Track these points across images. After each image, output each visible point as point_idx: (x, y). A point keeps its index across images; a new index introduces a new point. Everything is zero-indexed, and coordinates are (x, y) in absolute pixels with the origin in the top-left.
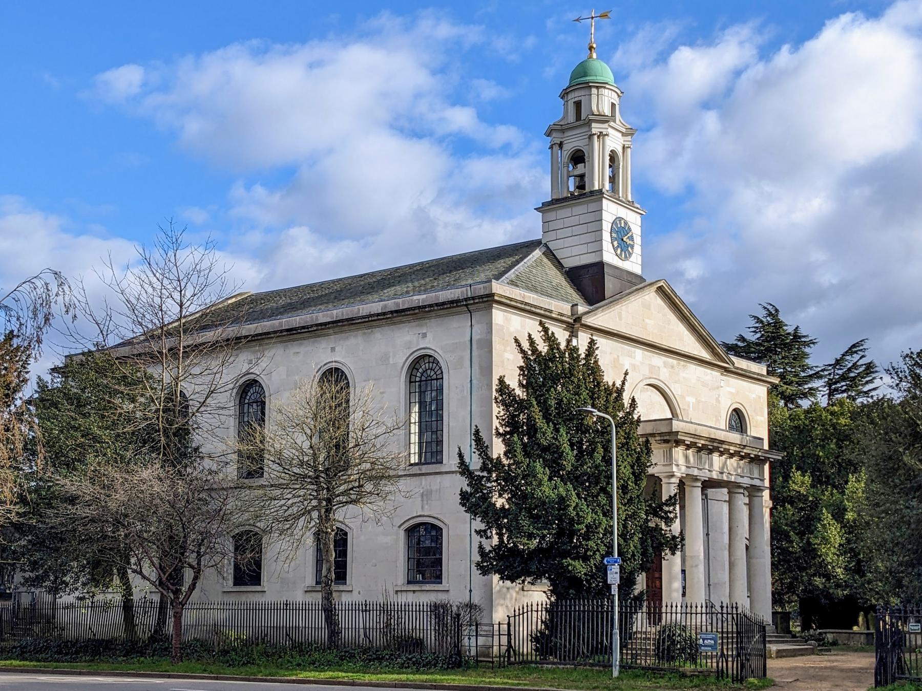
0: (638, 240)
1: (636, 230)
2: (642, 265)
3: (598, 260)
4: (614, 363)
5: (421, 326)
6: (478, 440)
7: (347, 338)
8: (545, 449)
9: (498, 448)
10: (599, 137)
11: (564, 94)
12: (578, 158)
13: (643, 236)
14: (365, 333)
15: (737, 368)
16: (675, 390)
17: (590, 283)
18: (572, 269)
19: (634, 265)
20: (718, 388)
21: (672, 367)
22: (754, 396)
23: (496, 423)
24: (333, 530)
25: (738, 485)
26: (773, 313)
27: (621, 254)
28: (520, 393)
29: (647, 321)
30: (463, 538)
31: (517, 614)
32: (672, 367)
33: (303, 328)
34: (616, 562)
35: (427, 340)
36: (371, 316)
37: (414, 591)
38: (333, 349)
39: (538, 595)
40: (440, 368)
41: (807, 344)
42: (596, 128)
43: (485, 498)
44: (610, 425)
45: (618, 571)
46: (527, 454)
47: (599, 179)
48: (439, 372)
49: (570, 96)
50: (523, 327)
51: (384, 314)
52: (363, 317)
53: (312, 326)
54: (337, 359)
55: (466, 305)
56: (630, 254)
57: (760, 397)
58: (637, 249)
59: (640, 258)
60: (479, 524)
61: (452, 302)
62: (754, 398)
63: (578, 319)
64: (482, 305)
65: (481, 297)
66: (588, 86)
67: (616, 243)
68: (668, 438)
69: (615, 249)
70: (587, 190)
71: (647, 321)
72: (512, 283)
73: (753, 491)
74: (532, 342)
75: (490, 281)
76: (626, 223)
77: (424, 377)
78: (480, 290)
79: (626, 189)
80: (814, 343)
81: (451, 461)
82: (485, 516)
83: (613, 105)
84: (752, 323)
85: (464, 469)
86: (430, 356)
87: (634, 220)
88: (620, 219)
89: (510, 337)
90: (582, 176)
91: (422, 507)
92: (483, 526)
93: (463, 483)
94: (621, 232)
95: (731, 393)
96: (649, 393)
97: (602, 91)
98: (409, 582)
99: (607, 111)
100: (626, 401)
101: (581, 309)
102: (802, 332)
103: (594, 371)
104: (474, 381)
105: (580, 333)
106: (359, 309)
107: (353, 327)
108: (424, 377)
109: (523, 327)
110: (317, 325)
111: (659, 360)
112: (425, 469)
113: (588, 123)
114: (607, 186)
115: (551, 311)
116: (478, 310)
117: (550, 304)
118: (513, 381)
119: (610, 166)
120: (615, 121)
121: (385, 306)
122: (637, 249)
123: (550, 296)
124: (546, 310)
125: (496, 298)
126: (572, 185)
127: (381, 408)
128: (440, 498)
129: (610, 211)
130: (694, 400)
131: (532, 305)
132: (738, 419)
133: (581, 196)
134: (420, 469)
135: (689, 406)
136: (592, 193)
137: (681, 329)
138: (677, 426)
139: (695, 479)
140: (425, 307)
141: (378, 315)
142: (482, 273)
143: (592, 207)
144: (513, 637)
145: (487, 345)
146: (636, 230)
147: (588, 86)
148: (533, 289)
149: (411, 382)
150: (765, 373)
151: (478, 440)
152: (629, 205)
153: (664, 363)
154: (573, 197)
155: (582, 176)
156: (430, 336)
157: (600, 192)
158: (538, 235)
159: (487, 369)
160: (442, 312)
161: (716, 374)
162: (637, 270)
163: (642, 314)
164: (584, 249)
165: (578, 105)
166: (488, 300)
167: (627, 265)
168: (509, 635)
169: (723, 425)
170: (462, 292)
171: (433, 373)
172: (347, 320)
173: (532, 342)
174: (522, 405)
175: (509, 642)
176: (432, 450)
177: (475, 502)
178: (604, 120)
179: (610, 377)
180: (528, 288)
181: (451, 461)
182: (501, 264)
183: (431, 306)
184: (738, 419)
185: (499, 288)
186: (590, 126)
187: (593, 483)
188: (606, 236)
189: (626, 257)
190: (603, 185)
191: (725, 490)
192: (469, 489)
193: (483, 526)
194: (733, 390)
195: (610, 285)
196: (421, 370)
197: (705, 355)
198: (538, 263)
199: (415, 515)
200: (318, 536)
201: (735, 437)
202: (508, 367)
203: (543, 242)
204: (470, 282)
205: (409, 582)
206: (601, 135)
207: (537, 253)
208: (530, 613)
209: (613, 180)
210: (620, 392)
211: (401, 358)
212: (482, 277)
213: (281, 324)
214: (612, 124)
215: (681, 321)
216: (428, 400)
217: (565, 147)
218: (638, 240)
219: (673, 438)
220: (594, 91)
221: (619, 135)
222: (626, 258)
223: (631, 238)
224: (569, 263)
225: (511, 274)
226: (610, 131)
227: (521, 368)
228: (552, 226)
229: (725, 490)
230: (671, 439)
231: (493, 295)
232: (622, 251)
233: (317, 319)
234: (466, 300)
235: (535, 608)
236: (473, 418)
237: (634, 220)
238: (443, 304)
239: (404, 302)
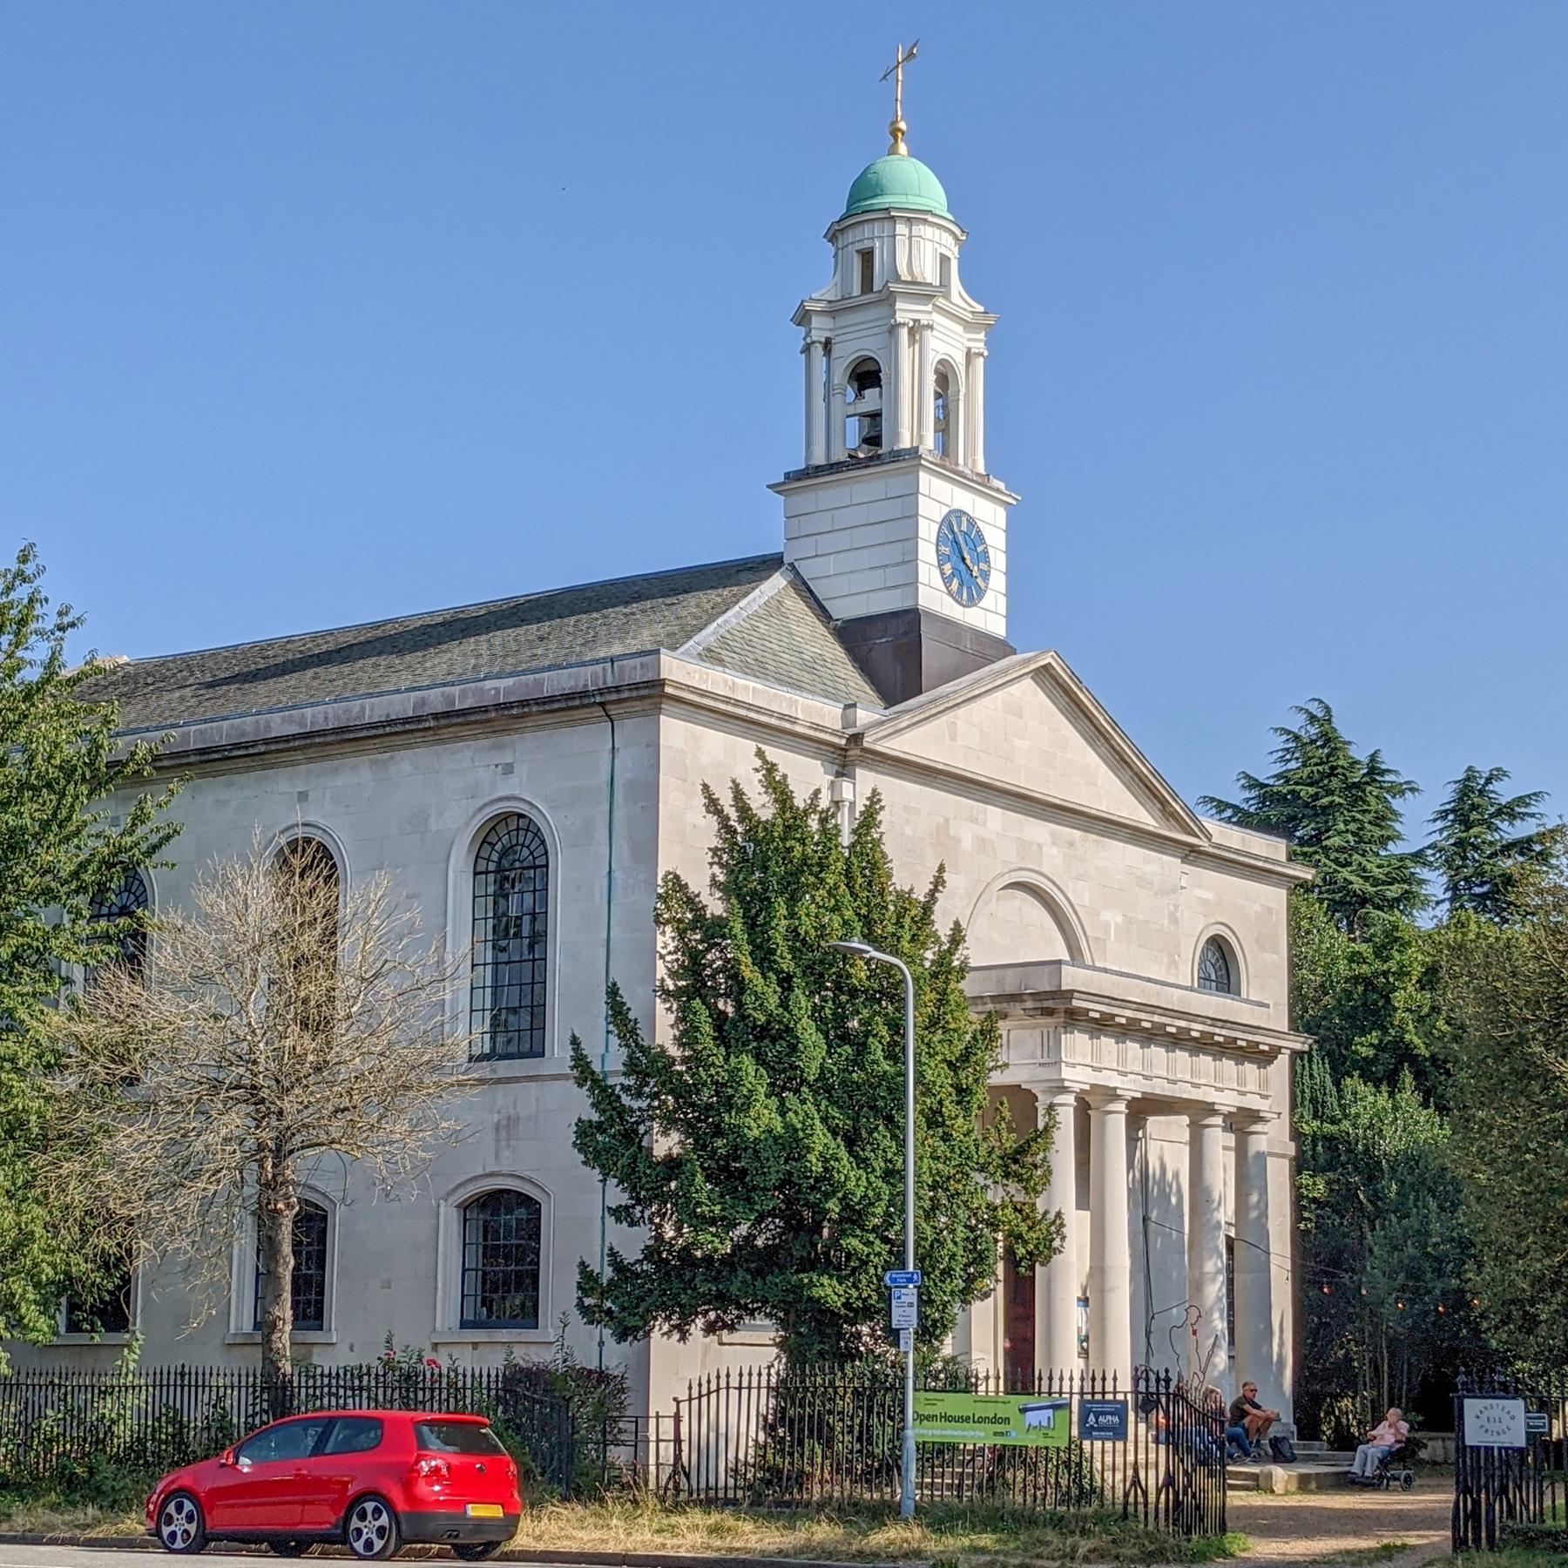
0: (998, 561)
1: (995, 540)
2: (1010, 617)
3: (907, 604)
4: (920, 838)
5: (499, 747)
6: (617, 1010)
7: (336, 771)
8: (763, 1032)
9: (664, 1031)
10: (912, 332)
11: (833, 236)
12: (867, 376)
13: (1009, 552)
14: (374, 763)
15: (1218, 846)
16: (1078, 895)
17: (891, 653)
18: (849, 622)
19: (989, 615)
20: (1174, 891)
21: (1071, 844)
22: (1257, 907)
23: (661, 971)
24: (288, 1205)
25: (1209, 1109)
26: (1323, 720)
27: (960, 592)
28: (715, 906)
29: (1018, 742)
30: (585, 1224)
31: (695, 1394)
32: (1071, 844)
33: (237, 746)
34: (910, 1280)
35: (514, 780)
36: (391, 723)
37: (475, 1345)
38: (303, 797)
39: (754, 1351)
40: (543, 842)
41: (1398, 790)
42: (905, 312)
43: (630, 1136)
44: (903, 981)
45: (914, 1300)
46: (722, 1039)
47: (912, 424)
48: (541, 850)
49: (851, 236)
50: (728, 760)
51: (419, 719)
52: (372, 726)
53: (255, 744)
54: (311, 819)
55: (602, 704)
56: (981, 593)
57: (1270, 910)
58: (998, 581)
59: (1003, 601)
60: (618, 1196)
61: (568, 697)
62: (1259, 915)
63: (856, 738)
64: (638, 706)
65: (635, 686)
66: (888, 216)
67: (948, 568)
68: (1049, 1004)
69: (947, 581)
70: (884, 449)
71: (1018, 742)
72: (710, 656)
73: (1242, 1122)
74: (738, 794)
75: (657, 652)
76: (972, 522)
77: (512, 859)
78: (635, 672)
79: (973, 452)
80: (1412, 790)
81: (559, 1054)
82: (629, 1178)
83: (944, 260)
84: (1279, 742)
85: (583, 1070)
86: (521, 816)
87: (991, 519)
88: (959, 513)
89: (699, 772)
90: (875, 416)
91: (497, 1156)
92: (624, 1199)
93: (581, 1105)
94: (961, 545)
95: (1206, 902)
96: (1018, 902)
97: (920, 229)
98: (464, 1325)
99: (930, 274)
100: (942, 927)
101: (863, 716)
102: (1386, 762)
103: (867, 861)
104: (617, 874)
105: (858, 771)
106: (363, 708)
107: (348, 748)
108: (512, 859)
109: (728, 760)
110: (267, 741)
111: (1039, 830)
112: (504, 1068)
113: (889, 299)
114: (929, 441)
115: (793, 720)
116: (629, 715)
117: (792, 703)
118: (701, 878)
119: (938, 396)
120: (947, 297)
121: (423, 702)
122: (998, 581)
123: (797, 686)
124: (782, 717)
125: (668, 690)
126: (853, 433)
127: (411, 936)
128: (536, 1134)
129: (937, 498)
130: (1119, 919)
131: (750, 707)
132: (1220, 965)
133: (874, 459)
134: (494, 1071)
135: (1107, 932)
136: (897, 456)
137: (1090, 759)
138: (1072, 978)
139: (1112, 1094)
140: (508, 706)
141: (406, 721)
142: (639, 630)
143: (896, 485)
144: (685, 1446)
145: (648, 792)
146: (995, 540)
147: (888, 216)
148: (755, 669)
149: (476, 874)
150: (1283, 858)
151: (617, 1010)
152: (978, 484)
153: (1053, 834)
154: (853, 462)
155: (875, 416)
156: (521, 770)
157: (914, 453)
158: (775, 545)
159: (647, 850)
160: (549, 719)
161: (1171, 863)
162: (997, 627)
163: (1002, 725)
164: (876, 579)
165: (867, 256)
166: (651, 694)
167: (972, 617)
168: (678, 1440)
169: (1186, 972)
170: (595, 676)
171: (526, 852)
172: (334, 731)
173: (738, 794)
174: (714, 930)
175: (678, 1457)
176: (517, 1024)
177: (609, 1141)
178: (924, 294)
179: (907, 875)
180: (746, 669)
181: (559, 1054)
182: (692, 603)
183: (524, 703)
184: (1220, 965)
185: (676, 668)
186: (892, 305)
187: (866, 1108)
188: (927, 552)
189: (971, 597)
190: (921, 437)
191: (1185, 1120)
192: (595, 1117)
193: (624, 1199)
194: (1209, 896)
195: (932, 654)
196: (498, 847)
197: (1145, 818)
198: (774, 608)
199: (480, 1172)
200: (265, 1218)
201: (1213, 1004)
202: (688, 850)
203: (786, 560)
204: (617, 649)
205: (464, 1325)
206: (916, 330)
207: (777, 582)
208: (723, 1393)
209: (945, 426)
210: (927, 909)
211: (459, 825)
212: (644, 640)
213: (186, 736)
214: (941, 302)
215: (1091, 742)
216: (513, 913)
217: (837, 350)
218: (998, 561)
219: (1060, 1005)
220: (901, 228)
221: (959, 329)
222: (972, 601)
223: (984, 558)
224: (844, 610)
225: (707, 636)
226: (937, 318)
227: (715, 851)
228: (810, 525)
229: (1185, 1120)
230: (1059, 1009)
231: (661, 683)
232: (961, 585)
233: (268, 727)
234: (601, 692)
235: (734, 1383)
236: (614, 958)
237: (991, 519)
238: (551, 699)
239: (463, 694)
